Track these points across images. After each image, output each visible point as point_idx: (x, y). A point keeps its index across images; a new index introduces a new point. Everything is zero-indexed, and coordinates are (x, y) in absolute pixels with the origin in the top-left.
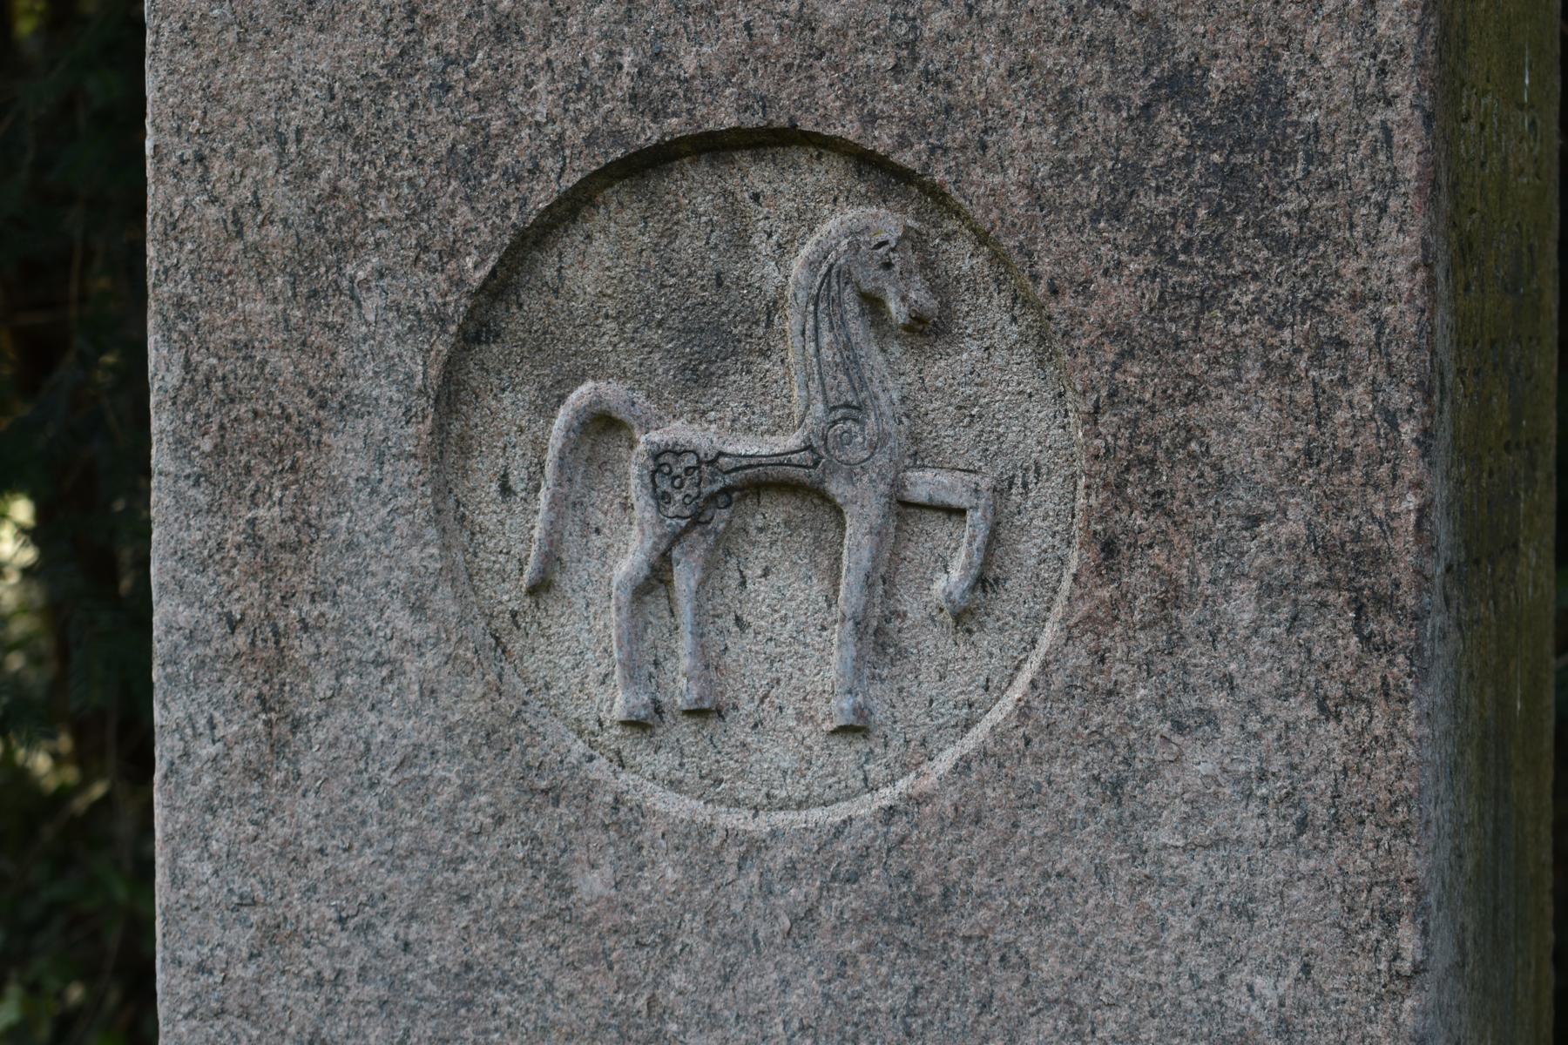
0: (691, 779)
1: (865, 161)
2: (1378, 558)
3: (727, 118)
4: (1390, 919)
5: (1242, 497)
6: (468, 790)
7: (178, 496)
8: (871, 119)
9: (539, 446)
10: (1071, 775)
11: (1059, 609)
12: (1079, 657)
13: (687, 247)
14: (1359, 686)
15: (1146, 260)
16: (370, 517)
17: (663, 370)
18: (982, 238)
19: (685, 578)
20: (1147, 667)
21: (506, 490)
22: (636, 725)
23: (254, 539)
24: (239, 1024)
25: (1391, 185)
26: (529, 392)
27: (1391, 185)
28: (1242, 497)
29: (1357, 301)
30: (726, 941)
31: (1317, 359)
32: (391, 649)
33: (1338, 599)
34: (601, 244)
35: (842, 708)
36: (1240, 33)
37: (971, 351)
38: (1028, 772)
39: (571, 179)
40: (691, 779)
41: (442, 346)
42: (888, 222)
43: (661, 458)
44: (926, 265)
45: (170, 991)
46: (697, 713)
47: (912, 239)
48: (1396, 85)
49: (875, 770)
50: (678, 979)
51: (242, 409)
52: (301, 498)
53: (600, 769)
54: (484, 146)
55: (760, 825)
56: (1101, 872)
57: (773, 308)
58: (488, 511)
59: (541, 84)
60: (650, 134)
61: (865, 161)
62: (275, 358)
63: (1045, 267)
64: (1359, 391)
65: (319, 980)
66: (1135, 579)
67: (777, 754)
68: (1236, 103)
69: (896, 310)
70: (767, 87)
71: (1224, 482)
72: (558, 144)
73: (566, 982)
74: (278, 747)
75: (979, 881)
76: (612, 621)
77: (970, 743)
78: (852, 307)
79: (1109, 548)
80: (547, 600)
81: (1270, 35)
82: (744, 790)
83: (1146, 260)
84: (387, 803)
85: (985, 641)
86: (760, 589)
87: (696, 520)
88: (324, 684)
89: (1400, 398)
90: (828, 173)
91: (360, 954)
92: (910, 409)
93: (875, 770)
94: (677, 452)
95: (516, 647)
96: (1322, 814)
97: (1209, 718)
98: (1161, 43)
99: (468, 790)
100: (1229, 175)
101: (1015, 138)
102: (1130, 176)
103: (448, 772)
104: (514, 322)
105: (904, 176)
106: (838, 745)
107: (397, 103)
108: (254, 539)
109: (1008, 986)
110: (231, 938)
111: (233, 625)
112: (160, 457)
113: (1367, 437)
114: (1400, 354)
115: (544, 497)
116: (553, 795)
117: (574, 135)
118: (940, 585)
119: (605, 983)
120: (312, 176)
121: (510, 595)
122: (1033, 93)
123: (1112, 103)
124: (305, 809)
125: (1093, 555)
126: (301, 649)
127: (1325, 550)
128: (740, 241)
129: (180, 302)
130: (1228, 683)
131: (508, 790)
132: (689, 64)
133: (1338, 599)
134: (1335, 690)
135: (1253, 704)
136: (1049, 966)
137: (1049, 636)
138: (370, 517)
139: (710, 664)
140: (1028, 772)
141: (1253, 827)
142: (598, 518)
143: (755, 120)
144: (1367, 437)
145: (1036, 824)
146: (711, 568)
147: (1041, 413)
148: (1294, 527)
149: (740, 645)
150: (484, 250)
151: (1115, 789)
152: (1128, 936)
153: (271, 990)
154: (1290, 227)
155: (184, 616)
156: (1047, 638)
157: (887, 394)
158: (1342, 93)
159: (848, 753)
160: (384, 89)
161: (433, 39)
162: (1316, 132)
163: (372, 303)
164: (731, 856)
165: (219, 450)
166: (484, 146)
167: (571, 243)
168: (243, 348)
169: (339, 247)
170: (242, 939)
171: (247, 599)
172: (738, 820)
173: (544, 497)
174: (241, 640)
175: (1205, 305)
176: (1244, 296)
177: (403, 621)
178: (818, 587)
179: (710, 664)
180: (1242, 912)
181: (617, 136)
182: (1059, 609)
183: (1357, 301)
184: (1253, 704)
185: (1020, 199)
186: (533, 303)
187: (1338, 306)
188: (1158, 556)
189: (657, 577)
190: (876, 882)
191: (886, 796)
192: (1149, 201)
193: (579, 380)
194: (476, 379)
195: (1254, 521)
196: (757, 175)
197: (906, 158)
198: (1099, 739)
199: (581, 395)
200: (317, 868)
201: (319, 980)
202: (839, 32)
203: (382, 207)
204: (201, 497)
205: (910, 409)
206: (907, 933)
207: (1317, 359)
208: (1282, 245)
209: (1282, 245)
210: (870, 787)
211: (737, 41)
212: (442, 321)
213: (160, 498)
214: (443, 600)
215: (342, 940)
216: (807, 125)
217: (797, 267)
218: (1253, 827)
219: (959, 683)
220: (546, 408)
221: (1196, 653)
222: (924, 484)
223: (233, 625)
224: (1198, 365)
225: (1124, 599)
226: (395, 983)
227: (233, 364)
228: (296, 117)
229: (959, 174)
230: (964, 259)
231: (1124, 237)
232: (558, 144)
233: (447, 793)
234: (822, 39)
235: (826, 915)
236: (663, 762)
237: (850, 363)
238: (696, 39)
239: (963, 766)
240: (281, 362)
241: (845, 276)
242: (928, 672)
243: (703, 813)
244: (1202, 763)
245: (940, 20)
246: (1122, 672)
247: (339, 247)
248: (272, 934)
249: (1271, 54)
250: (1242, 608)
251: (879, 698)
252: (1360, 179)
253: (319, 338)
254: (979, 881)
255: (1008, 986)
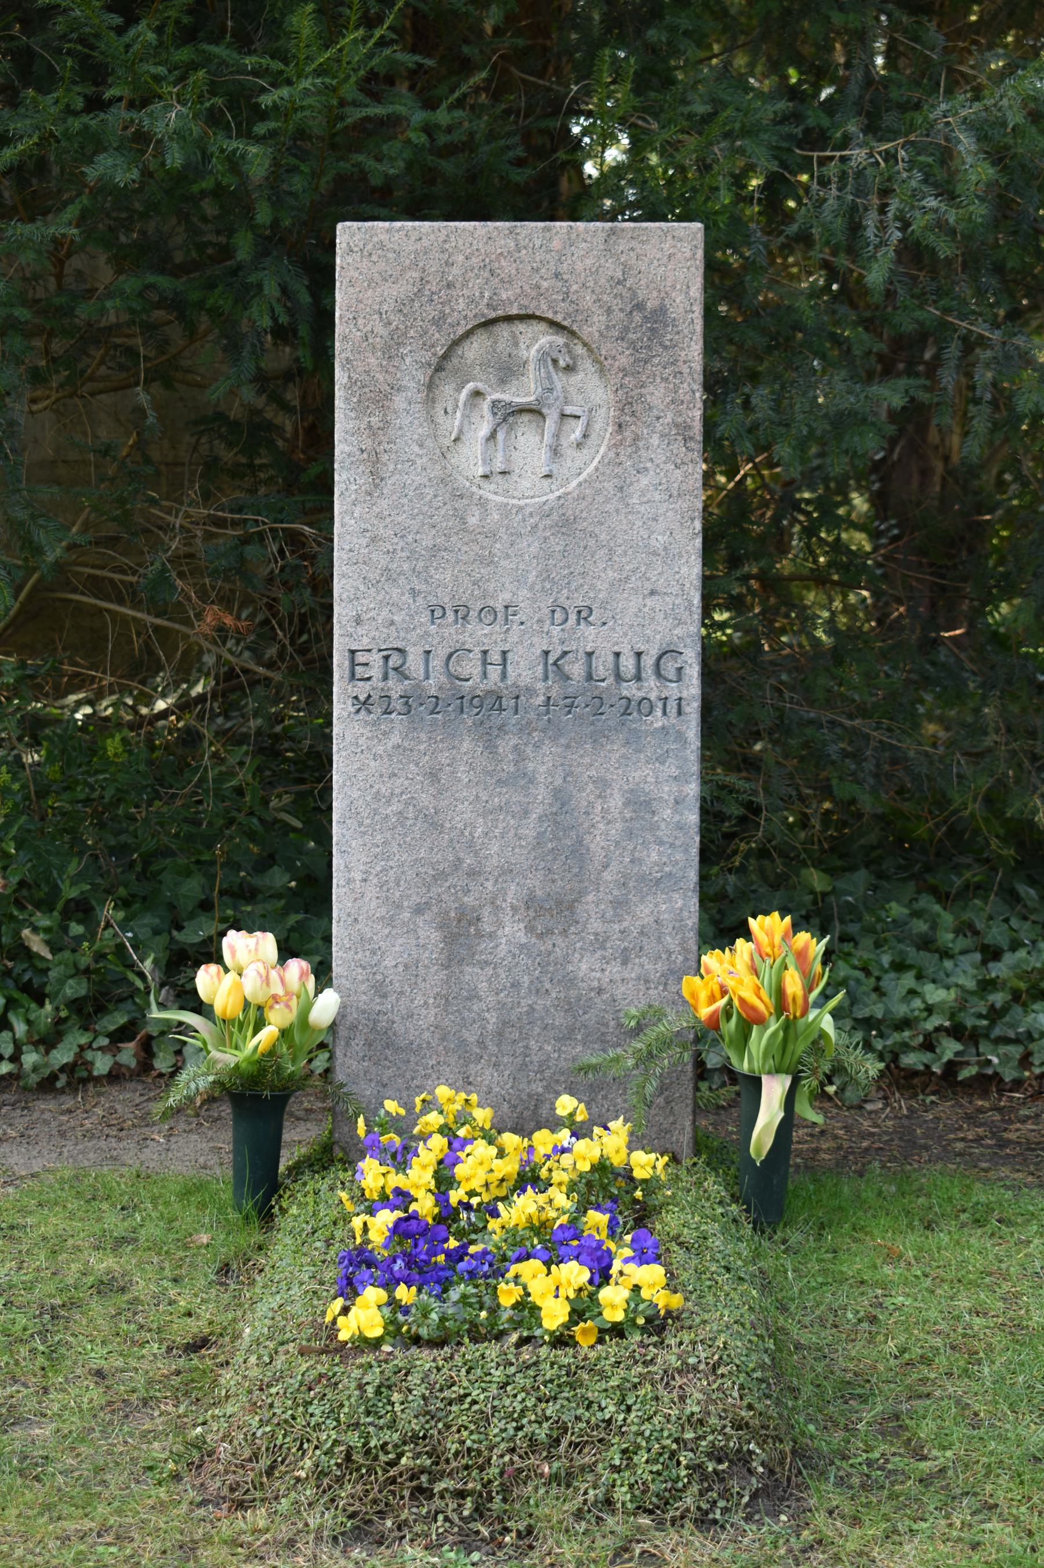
0: (500, 491)
1: (554, 324)
2: (690, 427)
3: (515, 311)
4: (693, 519)
5: (655, 412)
6: (435, 496)
7: (345, 415)
8: (556, 313)
9: (457, 401)
10: (609, 486)
11: (606, 442)
12: (612, 455)
13: (501, 346)
14: (686, 460)
15: (630, 351)
16: (406, 420)
17: (493, 380)
18: (585, 344)
19: (500, 436)
20: (630, 456)
21: (446, 412)
22: (485, 477)
23: (370, 426)
24: (362, 566)
25: (693, 333)
26: (454, 385)
27: (693, 333)
28: (655, 412)
29: (685, 362)
30: (512, 534)
31: (675, 377)
32: (412, 457)
33: (680, 438)
34: (475, 345)
35: (545, 471)
36: (655, 294)
37: (580, 376)
38: (598, 485)
39: (469, 327)
40: (500, 491)
41: (430, 372)
42: (560, 340)
43: (495, 403)
44: (569, 352)
45: (340, 558)
46: (503, 473)
47: (567, 345)
48: (695, 308)
49: (553, 487)
50: (498, 546)
51: (367, 390)
52: (385, 415)
53: (474, 489)
54: (443, 316)
55: (522, 503)
56: (617, 511)
57: (525, 363)
58: (440, 418)
59: (461, 300)
60: (493, 315)
61: (554, 324)
62: (378, 375)
63: (603, 352)
64: (685, 385)
65: (388, 552)
66: (627, 434)
67: (525, 484)
68: (654, 312)
69: (562, 363)
70: (526, 303)
71: (650, 408)
72: (465, 317)
73: (465, 548)
74: (376, 486)
75: (584, 515)
76: (479, 449)
77: (581, 478)
78: (550, 362)
79: (620, 426)
80: (459, 443)
81: (663, 294)
82: (516, 494)
83: (630, 351)
84: (411, 501)
85: (585, 451)
86: (521, 439)
87: (504, 420)
88: (391, 467)
89: (696, 387)
90: (542, 327)
91: (401, 544)
92: (565, 390)
93: (553, 487)
94: (499, 402)
95: (448, 456)
96: (675, 493)
97: (646, 469)
98: (634, 295)
99: (435, 496)
100: (652, 330)
101: (595, 319)
102: (626, 329)
103: (430, 492)
104: (449, 366)
105: (564, 328)
106: (544, 481)
107: (417, 304)
108: (370, 426)
109: (592, 542)
110: (360, 541)
111: (362, 451)
112: (338, 403)
113: (687, 397)
114: (696, 376)
115: (458, 414)
116: (461, 496)
117: (470, 315)
118: (573, 437)
119: (476, 548)
120: (390, 324)
121: (447, 442)
122: (600, 307)
123: (621, 310)
124: (384, 503)
125: (616, 427)
126: (384, 458)
127: (677, 425)
128: (516, 345)
129: (347, 359)
130: (651, 460)
131: (448, 495)
132: (504, 297)
133: (680, 438)
134: (679, 461)
135: (658, 466)
136: (603, 537)
137: (602, 450)
138: (406, 420)
139: (508, 460)
140: (598, 485)
141: (657, 497)
142: (473, 420)
143: (523, 312)
144: (687, 397)
145: (600, 499)
146: (508, 433)
147: (600, 391)
148: (669, 419)
149: (515, 454)
150: (443, 346)
151: (621, 489)
152: (624, 527)
153: (373, 556)
154: (668, 343)
155: (347, 449)
156: (602, 450)
157: (559, 385)
158: (681, 310)
159: (546, 482)
160: (413, 300)
161: (428, 287)
162: (674, 319)
163: (408, 360)
164: (514, 511)
165: (359, 401)
166: (443, 316)
167: (466, 344)
168: (367, 372)
169: (399, 344)
170: (364, 542)
171: (367, 444)
172: (515, 501)
173: (458, 414)
174: (365, 456)
175: (646, 363)
176: (656, 360)
177: (416, 449)
178: (538, 438)
179: (508, 460)
180: (655, 520)
181: (483, 315)
182: (606, 442)
183: (685, 362)
184: (658, 466)
185: (597, 335)
186: (455, 361)
187: (680, 363)
188: (633, 427)
189: (492, 436)
190: (555, 517)
191: (557, 494)
192: (631, 336)
193: (468, 382)
194: (437, 382)
195: (658, 418)
196: (521, 327)
197: (565, 323)
198: (617, 476)
199: (470, 386)
200: (388, 520)
201: (388, 552)
202: (547, 289)
203: (412, 333)
204: (353, 415)
205: (565, 390)
206: (564, 530)
207: (675, 377)
208: (666, 348)
209: (666, 348)
210: (552, 491)
211: (518, 291)
212: (430, 365)
213: (338, 415)
214: (429, 443)
215: (396, 540)
216: (538, 313)
217: (533, 351)
218: (657, 497)
219: (578, 463)
220: (459, 389)
221: (643, 452)
222: (569, 410)
223: (362, 451)
224: (644, 378)
225: (624, 439)
226: (413, 552)
227: (364, 376)
228: (385, 307)
229: (580, 327)
230: (580, 350)
231: (625, 345)
232: (465, 317)
233: (429, 497)
234: (542, 291)
235: (541, 526)
236: (493, 487)
237: (549, 377)
238: (506, 290)
239: (580, 484)
240: (380, 377)
241: (548, 354)
242: (569, 461)
243: (505, 500)
244: (644, 481)
245: (575, 287)
246: (622, 458)
247: (399, 344)
248: (373, 540)
249: (663, 299)
250: (655, 440)
251: (554, 467)
252: (686, 331)
253: (391, 369)
254: (584, 515)
255: (592, 542)
